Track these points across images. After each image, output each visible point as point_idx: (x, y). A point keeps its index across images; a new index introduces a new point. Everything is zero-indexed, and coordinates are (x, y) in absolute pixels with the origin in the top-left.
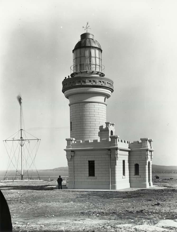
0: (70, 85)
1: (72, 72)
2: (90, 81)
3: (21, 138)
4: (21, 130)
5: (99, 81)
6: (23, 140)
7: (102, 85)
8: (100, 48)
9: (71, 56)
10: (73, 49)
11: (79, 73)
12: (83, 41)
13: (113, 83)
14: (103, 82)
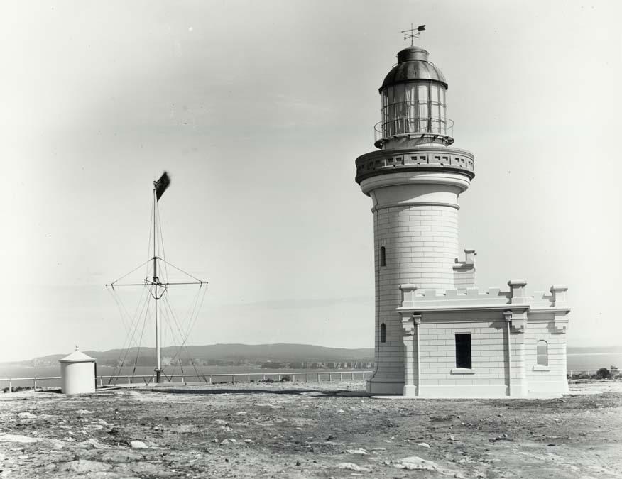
0: (371, 170)
1: (380, 137)
2: (415, 158)
3: (155, 278)
4: (155, 258)
5: (436, 157)
6: (158, 284)
7: (442, 164)
8: (441, 80)
9: (378, 100)
10: (381, 86)
11: (392, 140)
12: (402, 67)
13: (473, 157)
14: (444, 158)
